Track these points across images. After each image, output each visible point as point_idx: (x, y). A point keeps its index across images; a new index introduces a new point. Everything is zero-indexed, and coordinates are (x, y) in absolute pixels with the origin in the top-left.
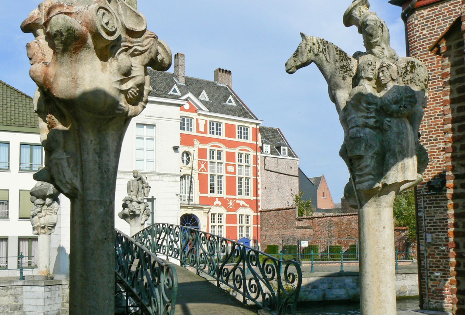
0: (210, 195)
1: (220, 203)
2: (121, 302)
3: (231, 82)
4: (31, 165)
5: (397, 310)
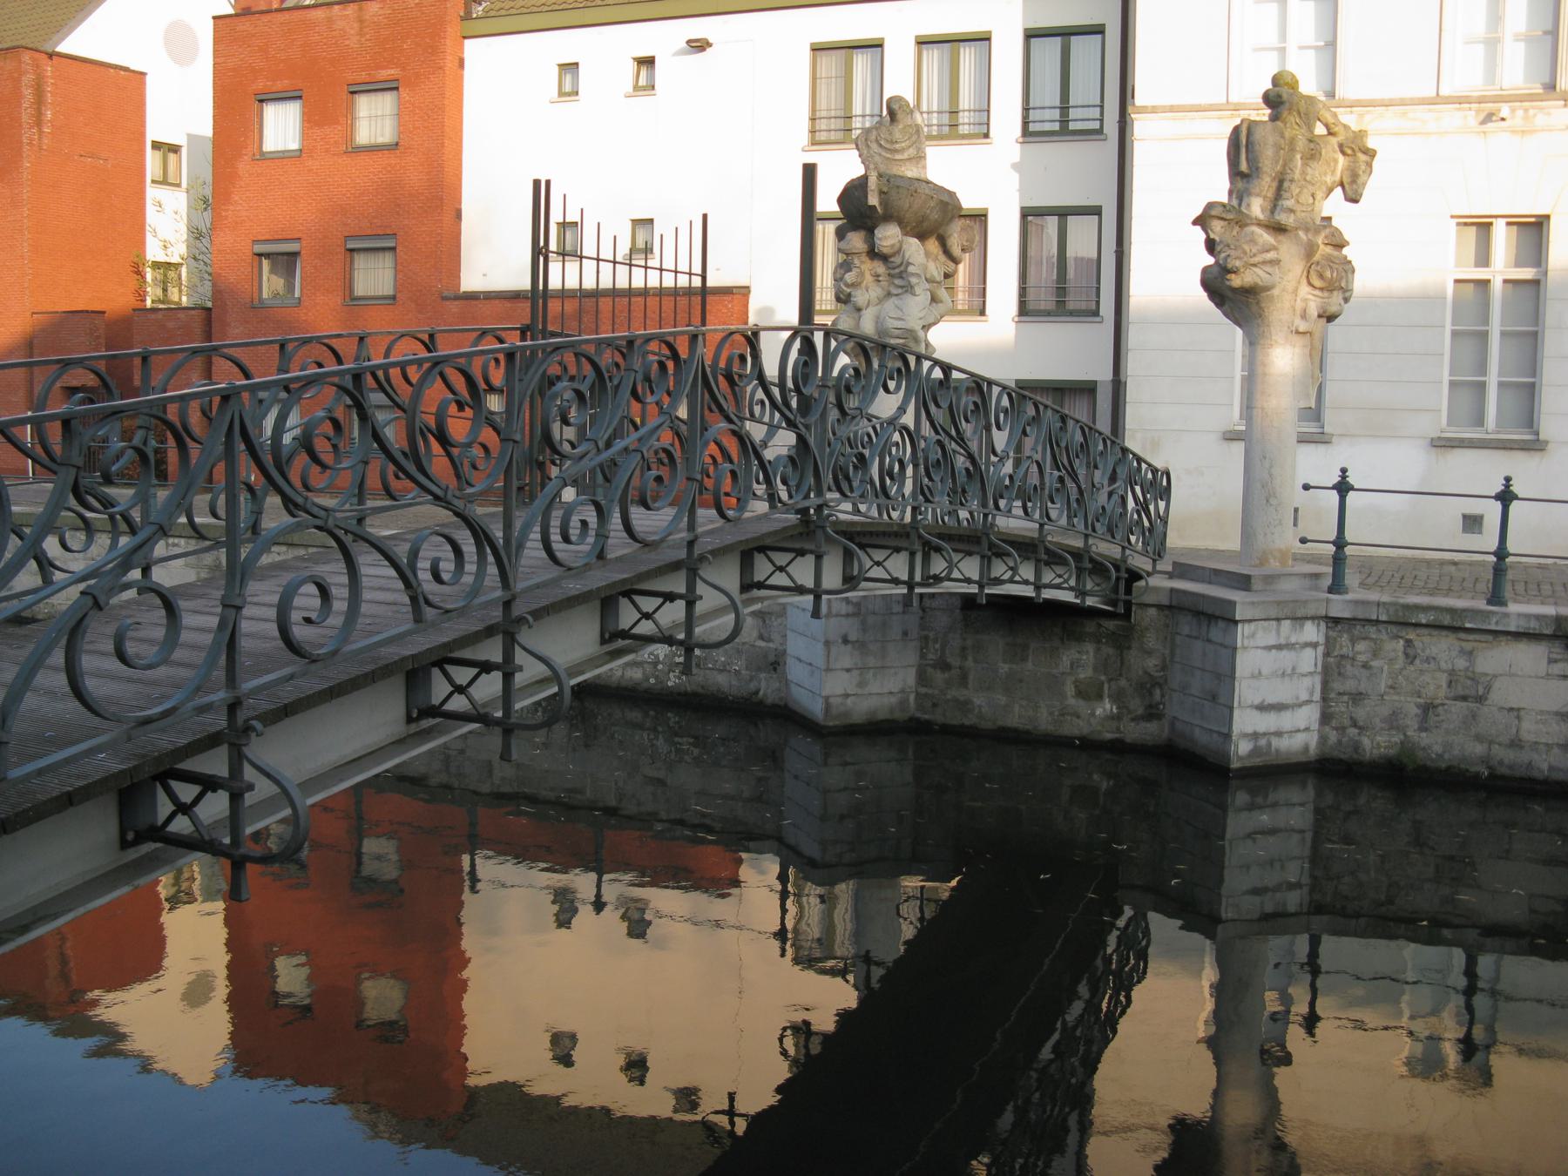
2: (936, 725)
4: (1064, 108)
5: (1488, 331)
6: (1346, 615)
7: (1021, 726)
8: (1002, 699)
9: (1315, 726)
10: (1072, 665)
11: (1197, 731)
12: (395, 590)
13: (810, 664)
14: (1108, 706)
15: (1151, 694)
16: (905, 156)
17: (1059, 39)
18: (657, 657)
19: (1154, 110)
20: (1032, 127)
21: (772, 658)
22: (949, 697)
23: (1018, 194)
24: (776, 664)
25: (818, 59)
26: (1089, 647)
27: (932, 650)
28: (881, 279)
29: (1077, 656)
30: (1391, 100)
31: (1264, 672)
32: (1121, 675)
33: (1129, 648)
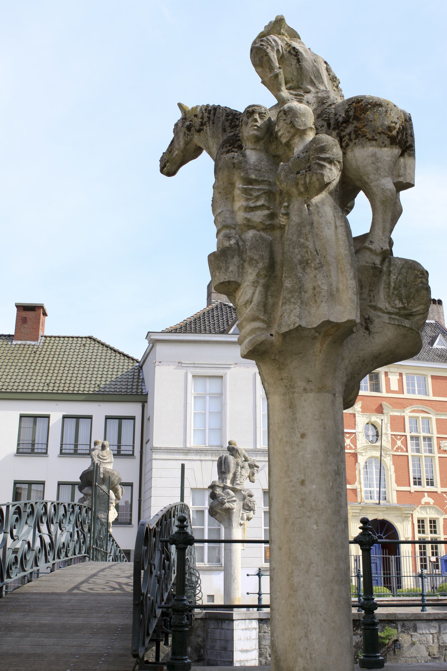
0: (414, 488)
1: (431, 501)
3: (443, 315)
4: (76, 446)
6: (265, 617)
9: (257, 658)
15: (200, 651)
16: (107, 461)
20: (21, 451)
31: (242, 638)
33: (191, 635)
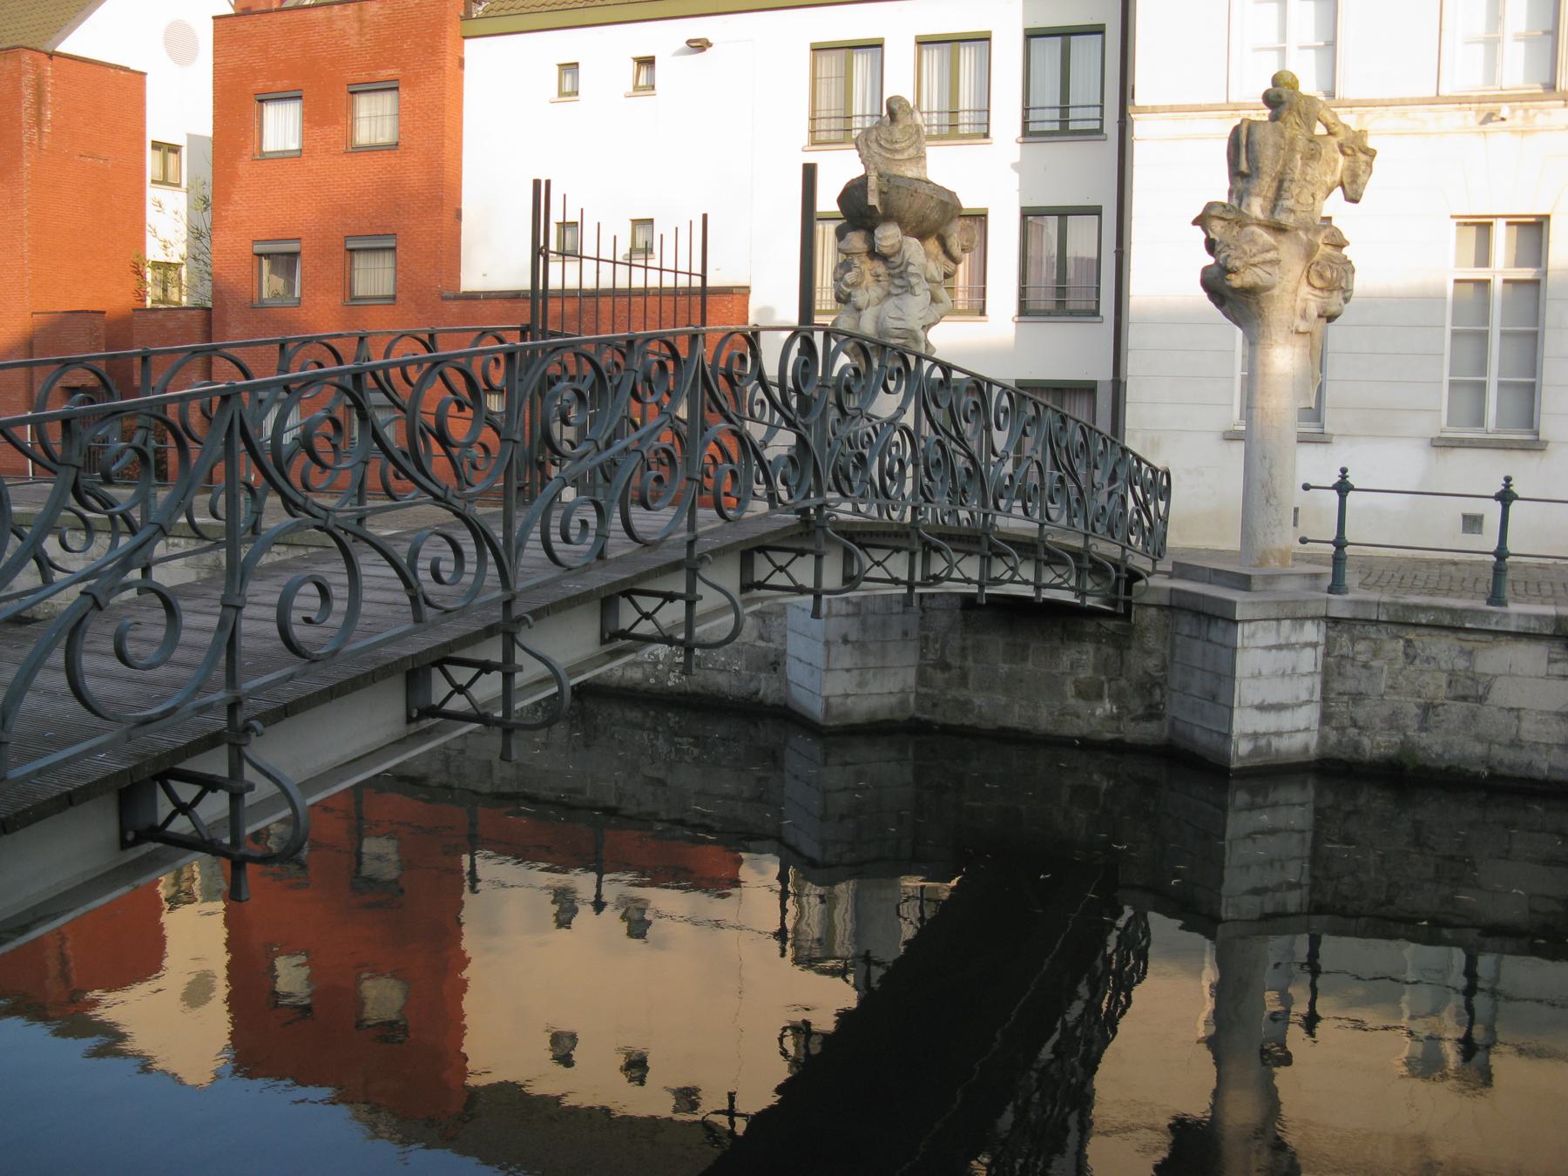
4: (1064, 108)
6: (1346, 615)
7: (1021, 726)
8: (1002, 699)
9: (1315, 726)
10: (1072, 665)
11: (1197, 731)
12: (395, 590)
13: (810, 664)
14: (1108, 706)
15: (1151, 694)
16: (905, 156)
17: (1059, 39)
18: (657, 657)
19: (1154, 110)
20: (1032, 127)
21: (772, 658)
22: (949, 697)
23: (1018, 194)
24: (776, 664)
25: (818, 59)
26: (1089, 647)
27: (932, 650)
28: (881, 279)
29: (1077, 656)
30: (1391, 100)
31: (1264, 672)
32: (1121, 675)
33: (1129, 648)
